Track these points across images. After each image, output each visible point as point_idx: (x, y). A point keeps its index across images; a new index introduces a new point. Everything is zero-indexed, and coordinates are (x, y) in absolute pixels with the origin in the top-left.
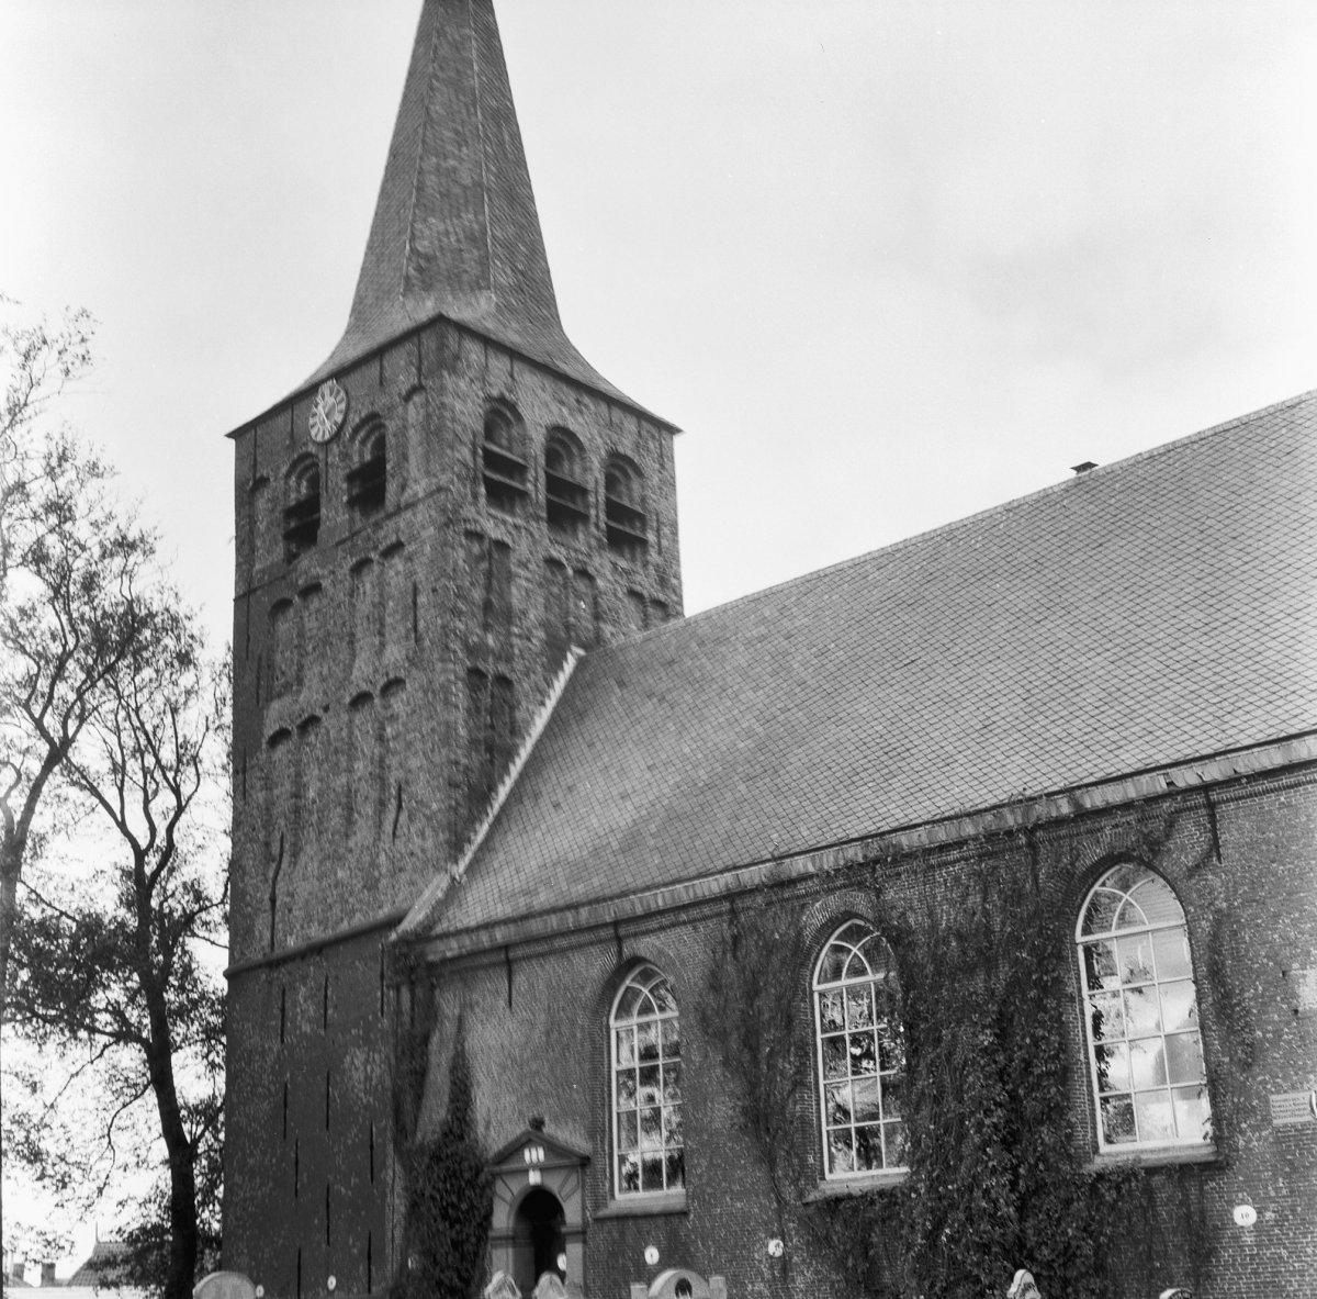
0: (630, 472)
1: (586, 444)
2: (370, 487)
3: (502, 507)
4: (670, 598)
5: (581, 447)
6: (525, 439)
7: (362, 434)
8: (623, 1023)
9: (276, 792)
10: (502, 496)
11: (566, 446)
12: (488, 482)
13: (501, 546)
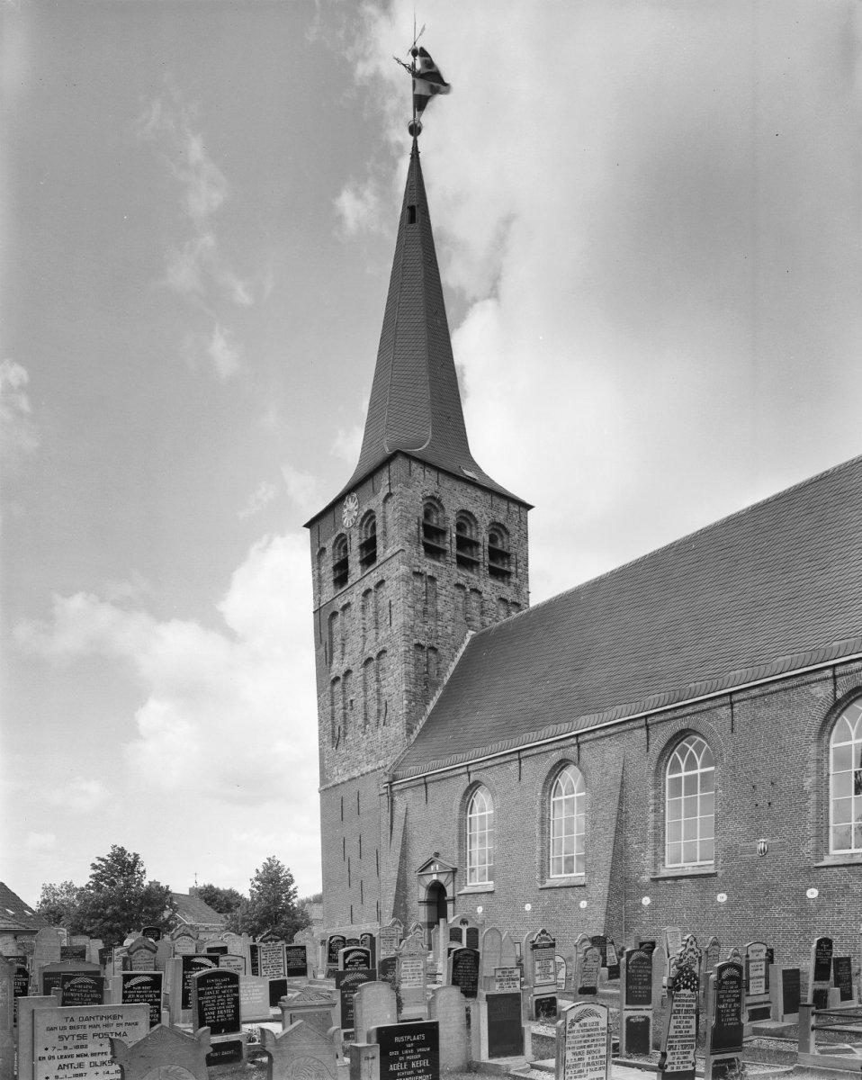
0: (504, 534)
1: (479, 519)
2: (369, 547)
3: (433, 558)
4: (522, 602)
5: (475, 519)
6: (446, 519)
7: (365, 523)
8: (554, 799)
9: (336, 707)
10: (433, 552)
11: (500, 533)
12: (425, 545)
13: (432, 579)
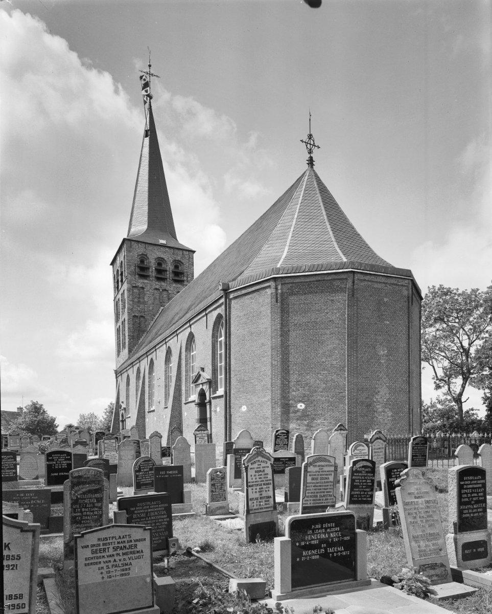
12: (139, 274)
